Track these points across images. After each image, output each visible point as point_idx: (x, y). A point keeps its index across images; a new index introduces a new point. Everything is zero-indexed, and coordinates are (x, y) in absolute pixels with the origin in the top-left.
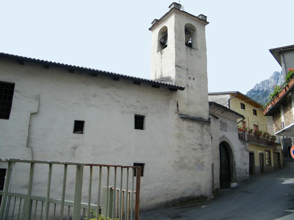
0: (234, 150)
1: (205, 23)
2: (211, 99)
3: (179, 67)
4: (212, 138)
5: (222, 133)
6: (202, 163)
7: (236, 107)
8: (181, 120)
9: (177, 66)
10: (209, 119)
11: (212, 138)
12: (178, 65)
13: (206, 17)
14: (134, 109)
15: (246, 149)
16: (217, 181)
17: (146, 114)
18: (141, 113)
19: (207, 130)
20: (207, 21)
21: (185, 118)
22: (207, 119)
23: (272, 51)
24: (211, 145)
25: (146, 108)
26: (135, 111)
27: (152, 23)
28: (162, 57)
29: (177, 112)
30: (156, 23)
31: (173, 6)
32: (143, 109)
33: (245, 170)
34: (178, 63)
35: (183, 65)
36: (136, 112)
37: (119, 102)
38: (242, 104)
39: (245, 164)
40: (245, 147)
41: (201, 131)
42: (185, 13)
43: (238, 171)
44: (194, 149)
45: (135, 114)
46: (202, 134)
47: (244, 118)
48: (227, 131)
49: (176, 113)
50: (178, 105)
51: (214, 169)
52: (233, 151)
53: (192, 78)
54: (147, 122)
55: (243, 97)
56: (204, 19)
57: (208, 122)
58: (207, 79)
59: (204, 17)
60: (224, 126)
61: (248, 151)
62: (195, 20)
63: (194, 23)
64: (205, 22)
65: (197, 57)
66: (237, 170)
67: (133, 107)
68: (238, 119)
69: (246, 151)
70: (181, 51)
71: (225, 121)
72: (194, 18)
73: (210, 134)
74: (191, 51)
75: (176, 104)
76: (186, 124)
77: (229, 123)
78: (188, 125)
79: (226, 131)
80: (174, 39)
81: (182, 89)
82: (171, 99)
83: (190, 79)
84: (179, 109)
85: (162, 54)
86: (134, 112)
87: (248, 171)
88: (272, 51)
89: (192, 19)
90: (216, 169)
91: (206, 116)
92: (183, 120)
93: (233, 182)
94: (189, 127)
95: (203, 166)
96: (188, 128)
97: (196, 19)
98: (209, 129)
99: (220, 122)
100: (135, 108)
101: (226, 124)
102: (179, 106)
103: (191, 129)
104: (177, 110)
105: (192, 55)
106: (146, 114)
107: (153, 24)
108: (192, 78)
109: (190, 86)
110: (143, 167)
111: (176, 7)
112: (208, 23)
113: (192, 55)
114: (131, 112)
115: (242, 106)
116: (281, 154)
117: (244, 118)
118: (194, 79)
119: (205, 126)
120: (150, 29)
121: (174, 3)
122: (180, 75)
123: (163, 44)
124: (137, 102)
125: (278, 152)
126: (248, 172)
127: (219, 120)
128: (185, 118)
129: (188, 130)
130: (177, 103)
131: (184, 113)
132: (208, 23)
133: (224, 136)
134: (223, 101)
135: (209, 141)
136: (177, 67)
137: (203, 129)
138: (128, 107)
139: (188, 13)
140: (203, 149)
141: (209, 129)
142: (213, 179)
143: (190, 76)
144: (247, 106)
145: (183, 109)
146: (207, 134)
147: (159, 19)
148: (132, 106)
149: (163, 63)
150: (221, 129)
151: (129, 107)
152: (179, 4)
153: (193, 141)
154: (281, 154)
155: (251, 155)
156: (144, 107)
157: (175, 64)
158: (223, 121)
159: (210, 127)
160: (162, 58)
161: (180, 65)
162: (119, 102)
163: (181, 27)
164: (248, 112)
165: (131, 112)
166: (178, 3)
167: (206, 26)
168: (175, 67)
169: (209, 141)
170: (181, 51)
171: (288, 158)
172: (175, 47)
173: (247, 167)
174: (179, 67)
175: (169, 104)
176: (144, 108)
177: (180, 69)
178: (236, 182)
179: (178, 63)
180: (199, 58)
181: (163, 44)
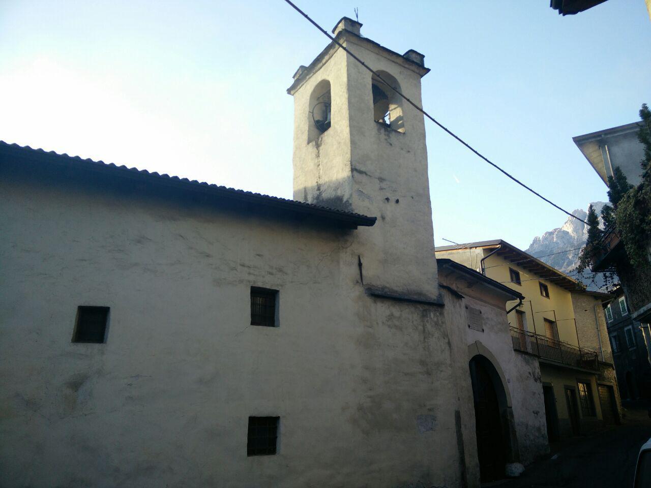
0: (505, 378)
1: (422, 72)
2: (439, 255)
3: (361, 172)
4: (449, 343)
5: (472, 336)
6: (430, 410)
7: (499, 273)
8: (369, 301)
9: (356, 170)
10: (440, 296)
11: (449, 343)
12: (358, 168)
13: (423, 56)
14: (249, 274)
15: (534, 376)
16: (472, 461)
17: (282, 286)
18: (267, 282)
19: (436, 324)
20: (426, 66)
21: (379, 295)
22: (435, 298)
23: (580, 141)
24: (448, 362)
25: (280, 270)
26: (252, 278)
27: (294, 77)
28: (319, 152)
29: (360, 281)
30: (304, 74)
31: (341, 27)
32: (271, 274)
33: (539, 429)
34: (358, 165)
35: (368, 167)
36: (254, 282)
37: (208, 256)
38: (512, 271)
39: (537, 413)
40: (531, 371)
41: (421, 328)
42: (370, 46)
43: (520, 431)
44: (406, 374)
45: (251, 287)
46: (425, 334)
47: (521, 297)
48: (483, 330)
49: (358, 282)
50: (360, 265)
51: (462, 426)
52: (503, 380)
53: (393, 199)
54: (285, 306)
55: (514, 253)
56: (417, 60)
57: (439, 305)
58: (429, 202)
59: (418, 57)
60: (475, 318)
61: (538, 381)
62: (397, 63)
63: (393, 70)
64: (421, 69)
65: (402, 149)
66: (517, 428)
67: (246, 269)
68: (508, 302)
69: (536, 380)
70: (364, 136)
71: (478, 307)
72: (393, 58)
73: (445, 335)
74: (388, 136)
75: (356, 261)
76: (382, 310)
77: (488, 311)
78: (388, 313)
79: (481, 330)
80: (345, 106)
81: (370, 222)
82: (343, 248)
83: (388, 201)
84: (364, 272)
85: (318, 146)
86: (249, 281)
87: (544, 431)
88: (580, 141)
89: (389, 59)
90: (465, 425)
91: (431, 289)
92: (375, 302)
93: (513, 462)
94: (391, 317)
95: (434, 418)
96: (388, 321)
97: (399, 60)
98: (440, 322)
99: (465, 309)
100: (252, 271)
101: (481, 313)
102: (308, 16)
103: (397, 323)
104: (359, 276)
105: (391, 144)
106: (280, 287)
107: (296, 78)
108: (393, 199)
109: (388, 219)
110: (458, 439)
111: (350, 29)
112: (428, 70)
113: (391, 144)
114: (241, 281)
115: (514, 276)
116: (616, 389)
117: (524, 298)
118: (397, 201)
119: (430, 314)
120: (289, 91)
121: (345, 19)
122: (364, 191)
123: (321, 125)
124: (258, 257)
125: (608, 384)
126: (546, 432)
127: (464, 302)
128: (379, 295)
129: (389, 326)
130: (357, 257)
131: (378, 283)
132: (428, 70)
133: (477, 344)
134: (472, 260)
135: (442, 351)
136: (355, 172)
137: (427, 321)
138: (234, 269)
139: (377, 45)
140: (428, 373)
141: (442, 323)
142: (462, 453)
143: (389, 195)
144: (524, 276)
145: (373, 272)
146: (436, 335)
147: (307, 65)
148: (243, 265)
149: (321, 166)
150: (469, 326)
151: (236, 270)
152: (357, 23)
153: (404, 354)
154: (616, 389)
155: (548, 391)
156: (276, 269)
157: (351, 165)
158: (472, 306)
159: (444, 317)
160: (319, 156)
161: (363, 169)
162: (208, 256)
163: (364, 78)
164: (529, 286)
165: (241, 281)
166: (355, 19)
167: (424, 80)
168: (350, 172)
169: (442, 351)
170: (364, 136)
171: (628, 400)
172: (350, 126)
173: (543, 420)
174: (361, 172)
175: (338, 262)
176: (274, 271)
177: (363, 178)
178: (519, 462)
179: (358, 165)
180: (409, 152)
181: (321, 125)
